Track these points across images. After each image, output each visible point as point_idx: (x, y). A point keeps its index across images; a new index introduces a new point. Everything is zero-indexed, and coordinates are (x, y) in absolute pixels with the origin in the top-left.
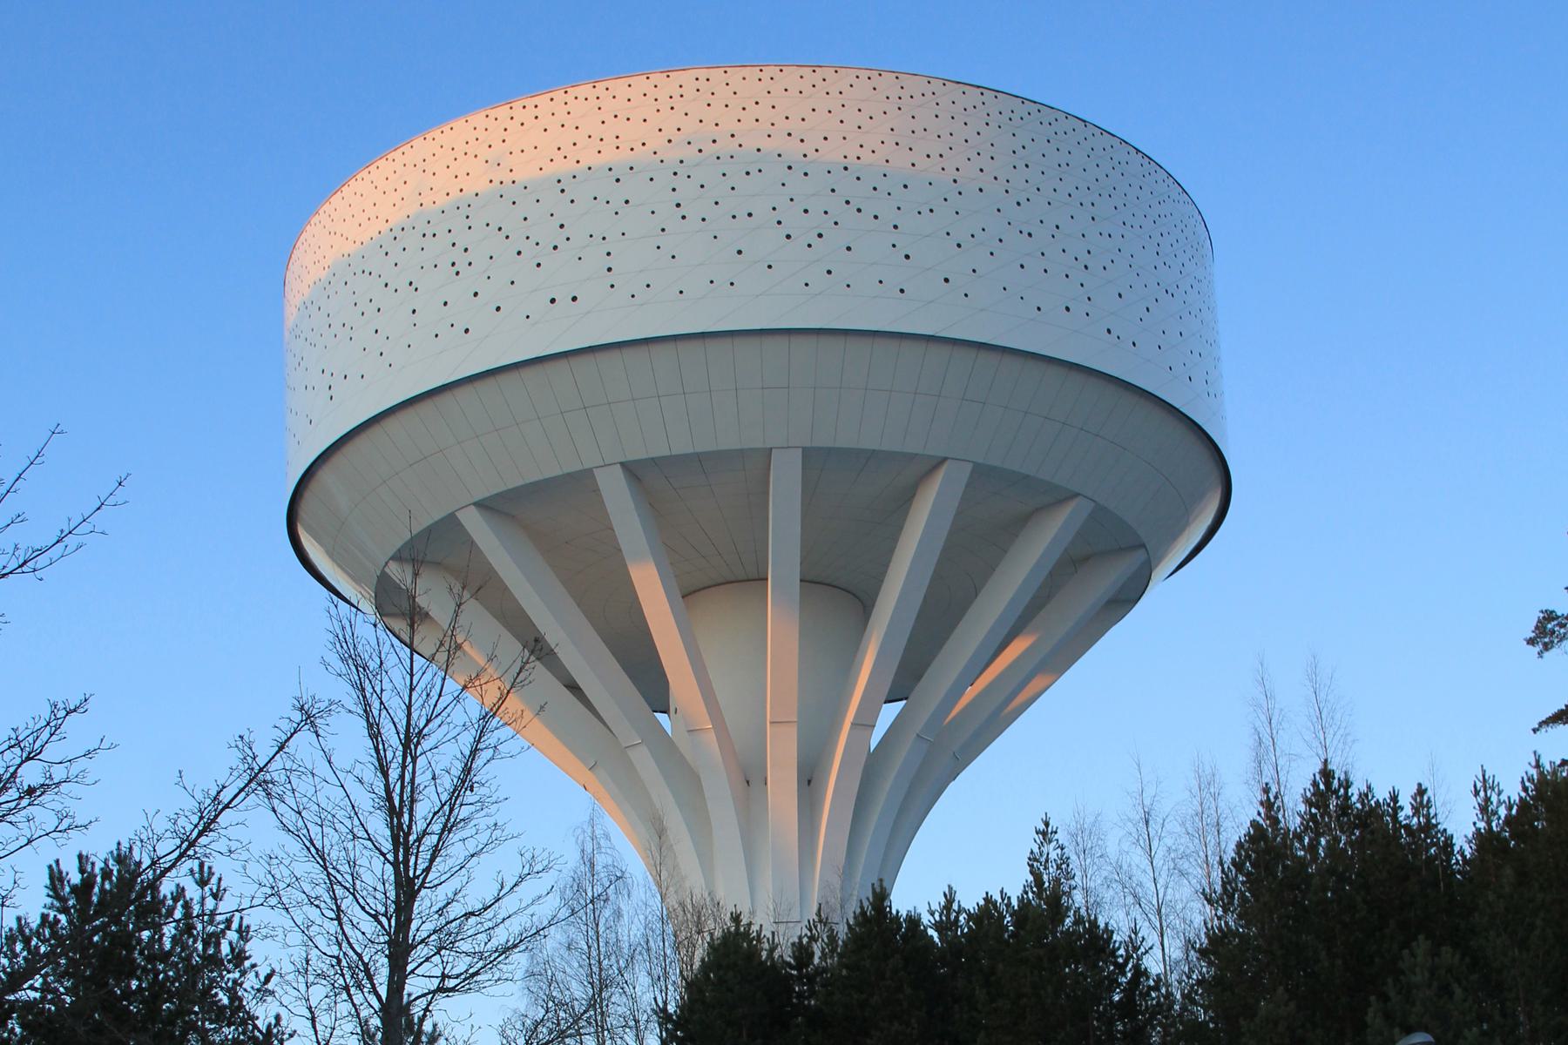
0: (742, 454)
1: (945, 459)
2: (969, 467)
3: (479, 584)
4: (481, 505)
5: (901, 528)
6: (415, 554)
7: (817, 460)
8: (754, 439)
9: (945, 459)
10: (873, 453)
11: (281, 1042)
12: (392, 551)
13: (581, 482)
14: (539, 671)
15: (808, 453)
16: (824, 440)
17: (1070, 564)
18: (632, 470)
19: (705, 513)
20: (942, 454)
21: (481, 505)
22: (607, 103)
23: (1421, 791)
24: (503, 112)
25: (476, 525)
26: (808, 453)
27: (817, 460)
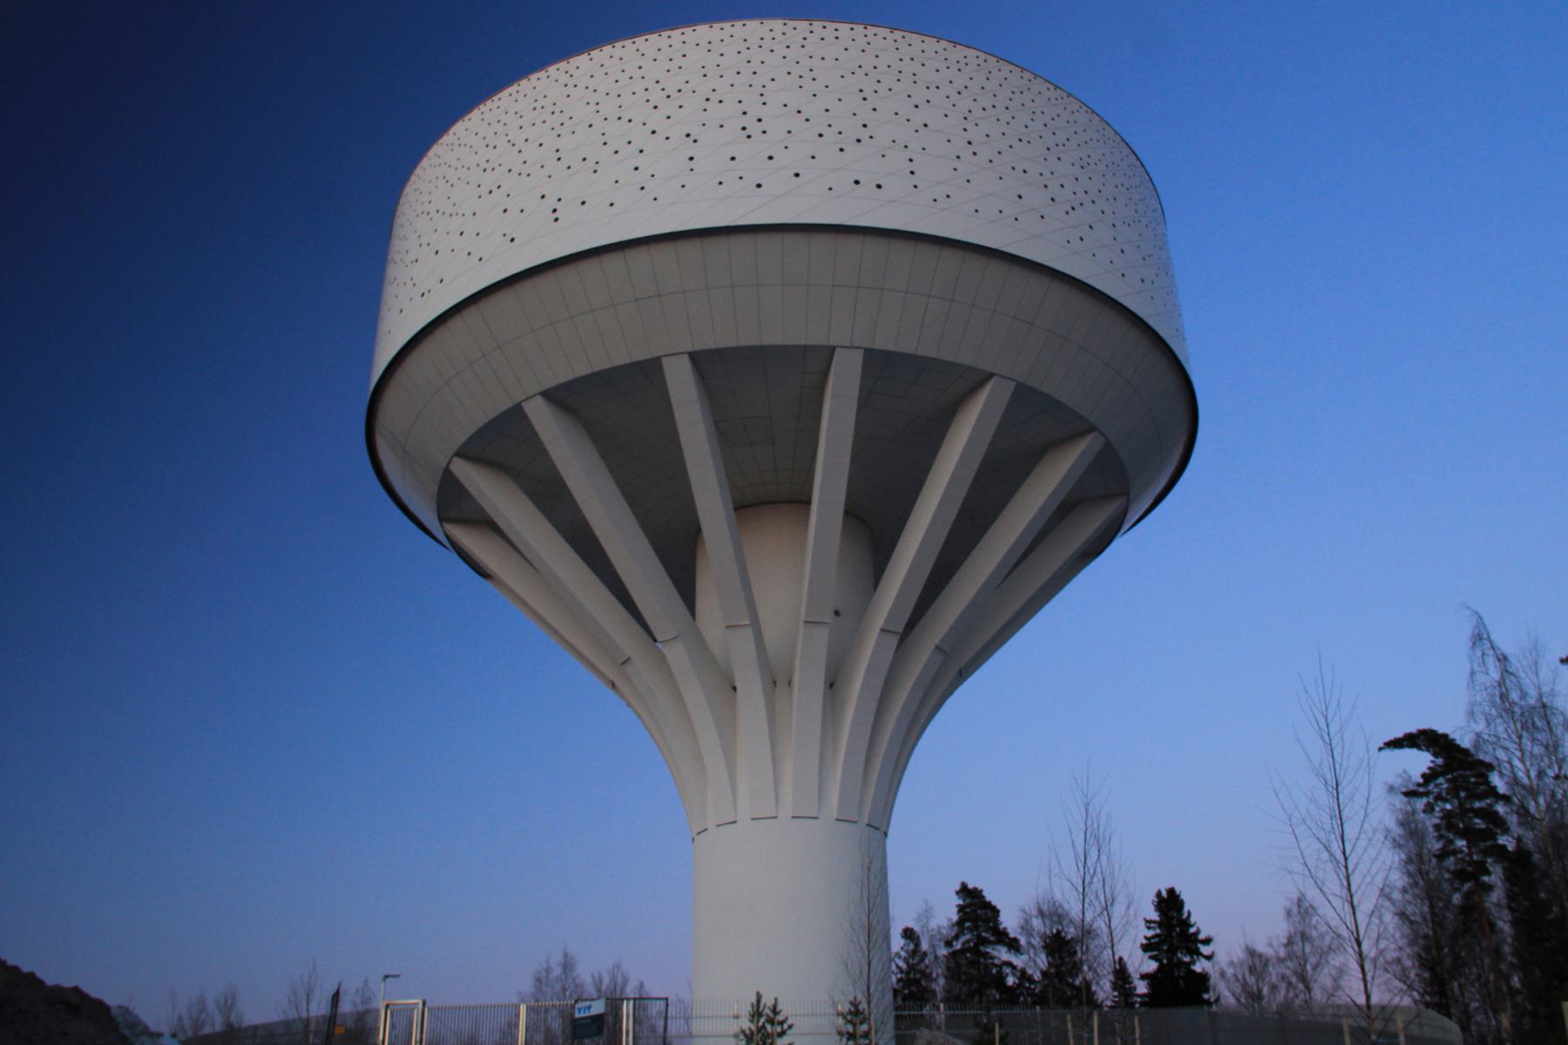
0: (805, 350)
1: (991, 376)
2: (1013, 384)
3: (551, 497)
4: (546, 395)
5: (1027, 474)
6: (478, 449)
7: (879, 364)
8: (816, 338)
9: (991, 376)
10: (1059, 403)
11: (1562, 826)
12: (455, 446)
13: (648, 372)
14: (895, 641)
15: (871, 355)
16: (884, 343)
17: (1065, 509)
18: (697, 358)
19: (761, 389)
20: (989, 369)
21: (546, 395)
22: (904, 48)
23: (1170, 904)
24: (803, 25)
25: (542, 417)
26: (871, 355)
27: (879, 364)
